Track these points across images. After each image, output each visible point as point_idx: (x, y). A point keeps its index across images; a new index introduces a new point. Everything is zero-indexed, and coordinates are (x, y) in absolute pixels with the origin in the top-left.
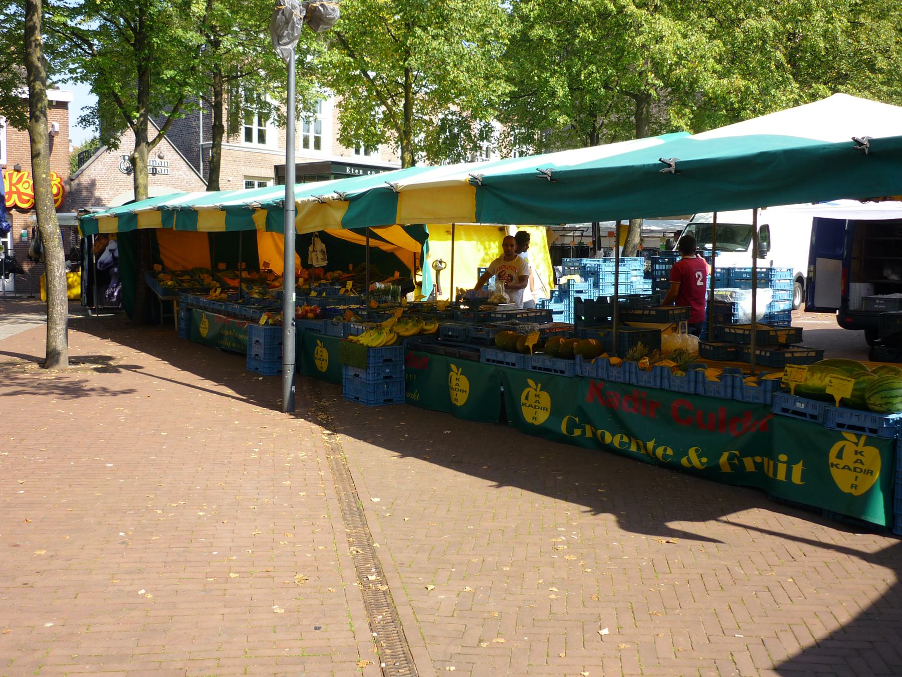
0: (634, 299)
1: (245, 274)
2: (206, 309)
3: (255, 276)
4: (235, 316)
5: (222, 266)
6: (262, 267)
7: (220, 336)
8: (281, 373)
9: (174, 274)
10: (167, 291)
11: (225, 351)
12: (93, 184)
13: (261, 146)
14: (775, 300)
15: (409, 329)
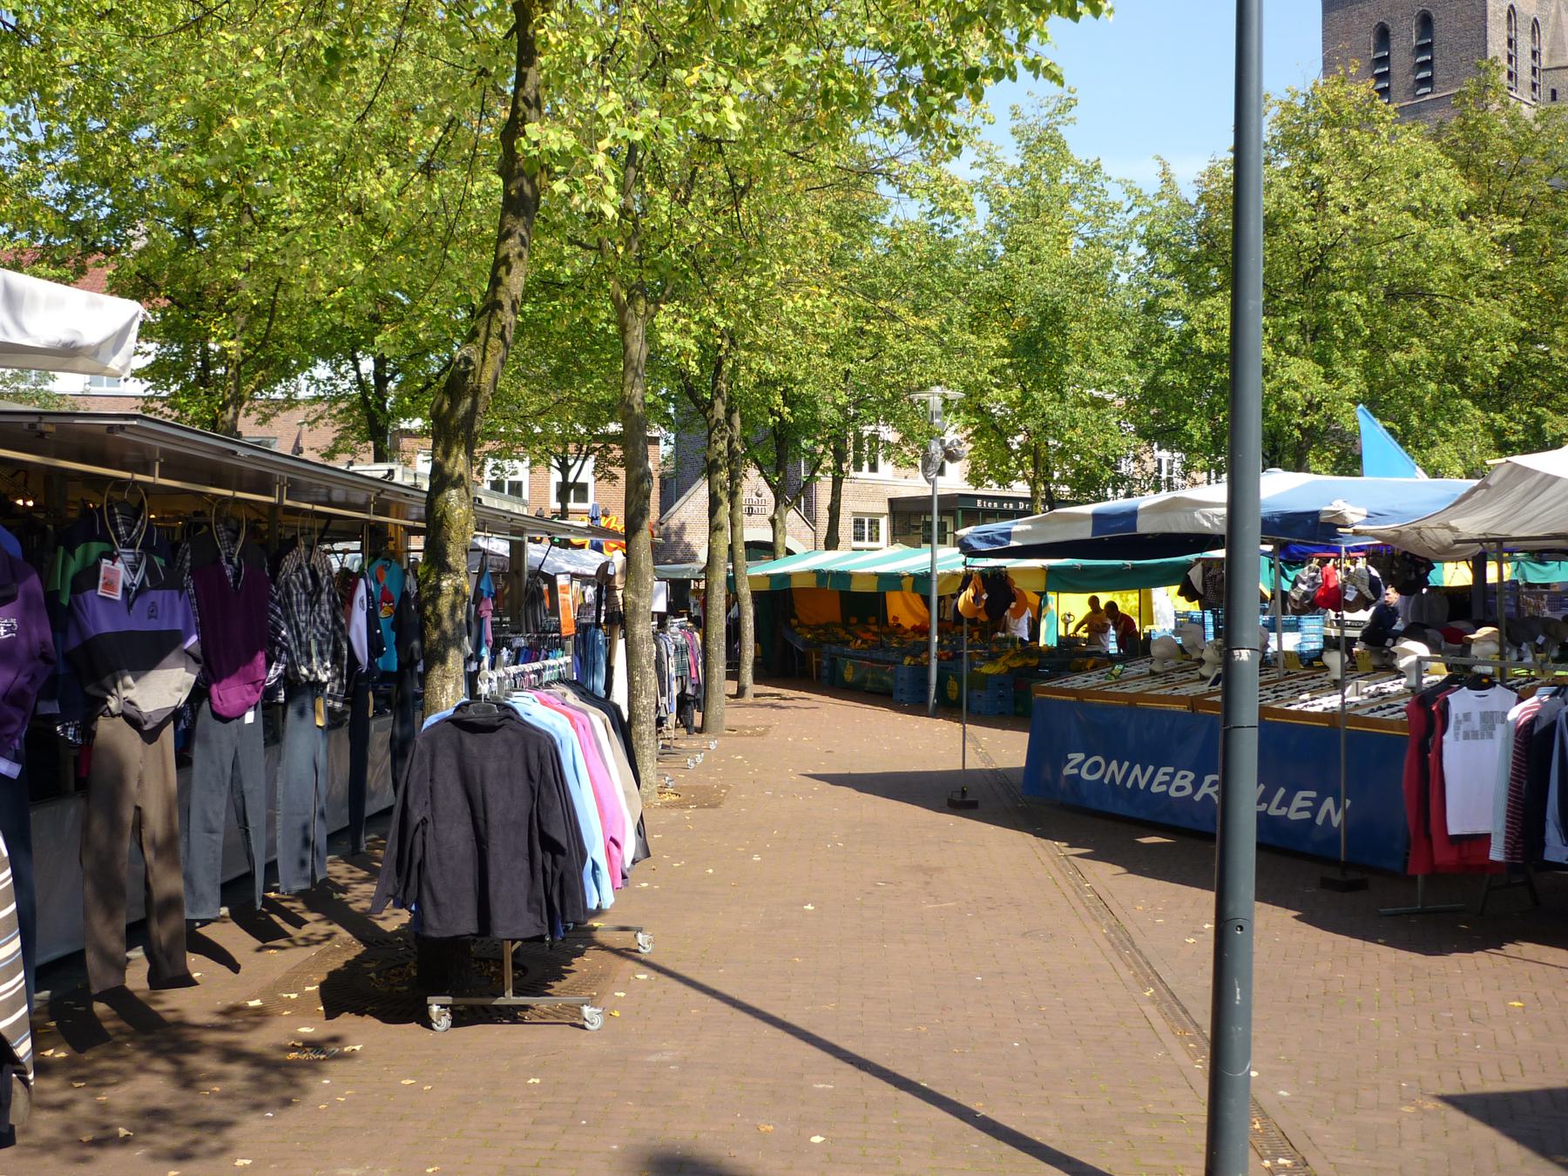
0: (426, 544)
1: (874, 628)
2: (850, 657)
3: (886, 629)
4: (878, 661)
5: (853, 620)
6: (891, 621)
7: (864, 680)
8: (926, 692)
9: (811, 629)
10: (807, 643)
11: (870, 692)
12: (682, 528)
13: (873, 475)
14: (1304, 641)
15: (1017, 663)
